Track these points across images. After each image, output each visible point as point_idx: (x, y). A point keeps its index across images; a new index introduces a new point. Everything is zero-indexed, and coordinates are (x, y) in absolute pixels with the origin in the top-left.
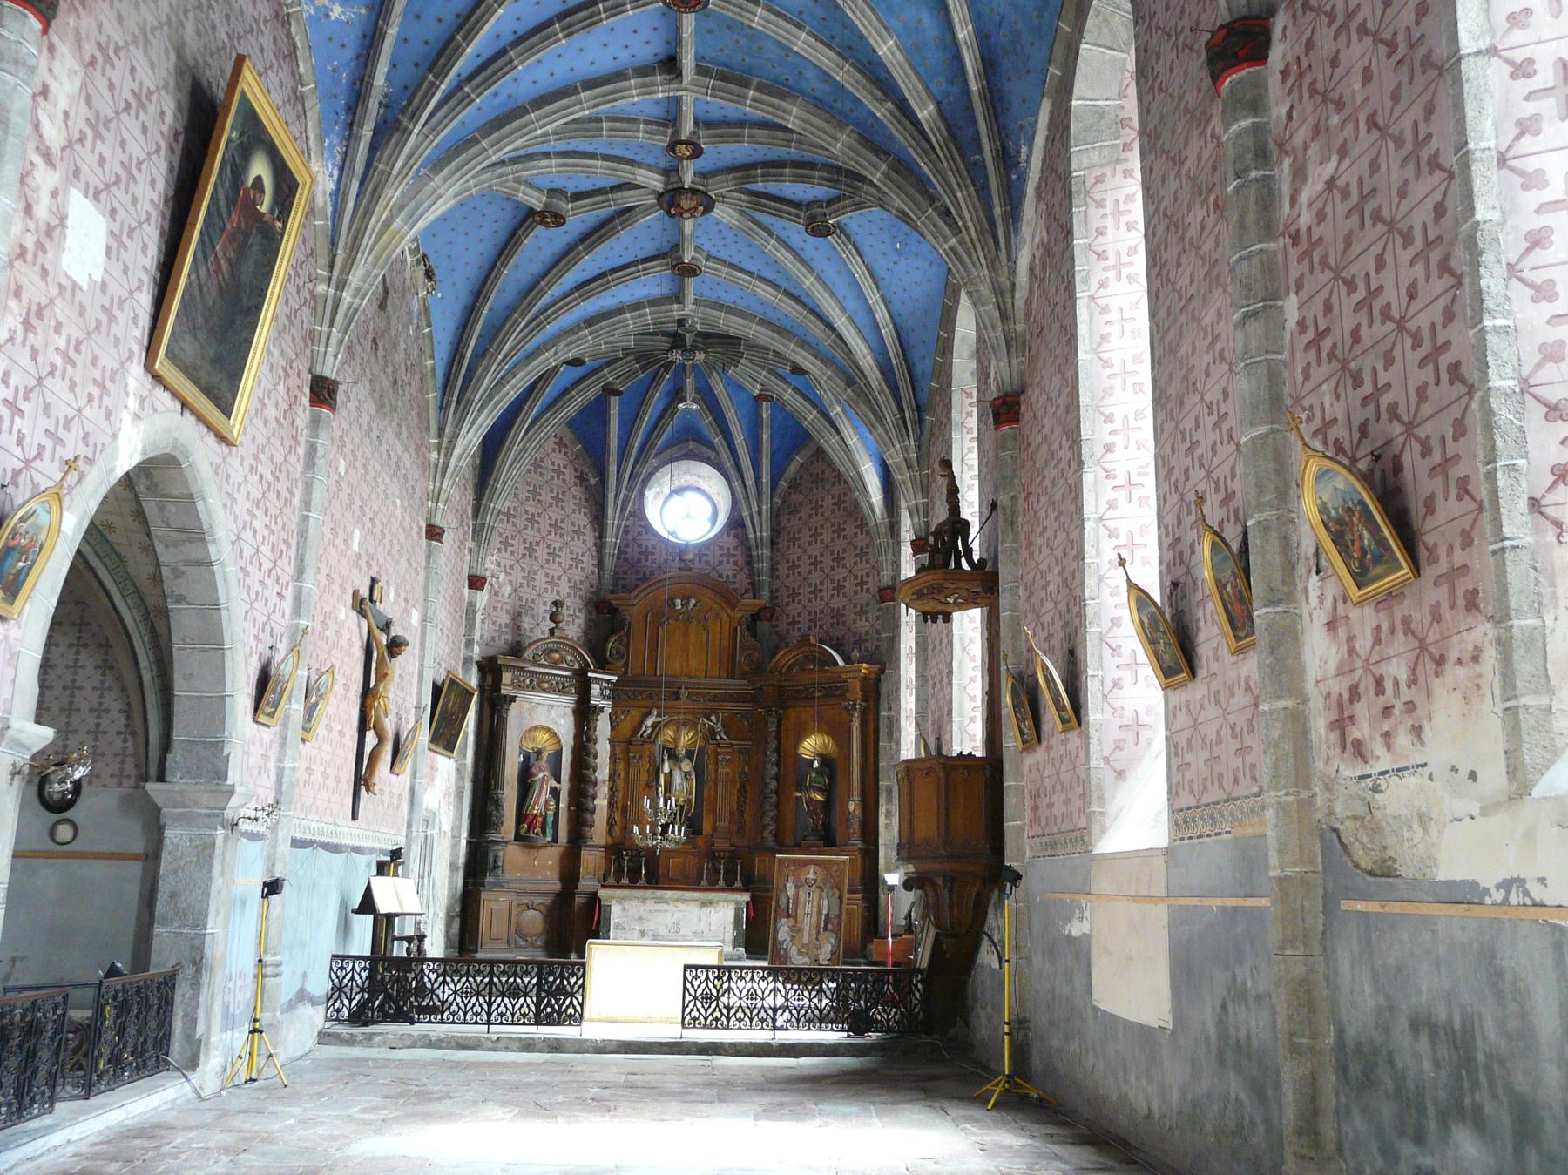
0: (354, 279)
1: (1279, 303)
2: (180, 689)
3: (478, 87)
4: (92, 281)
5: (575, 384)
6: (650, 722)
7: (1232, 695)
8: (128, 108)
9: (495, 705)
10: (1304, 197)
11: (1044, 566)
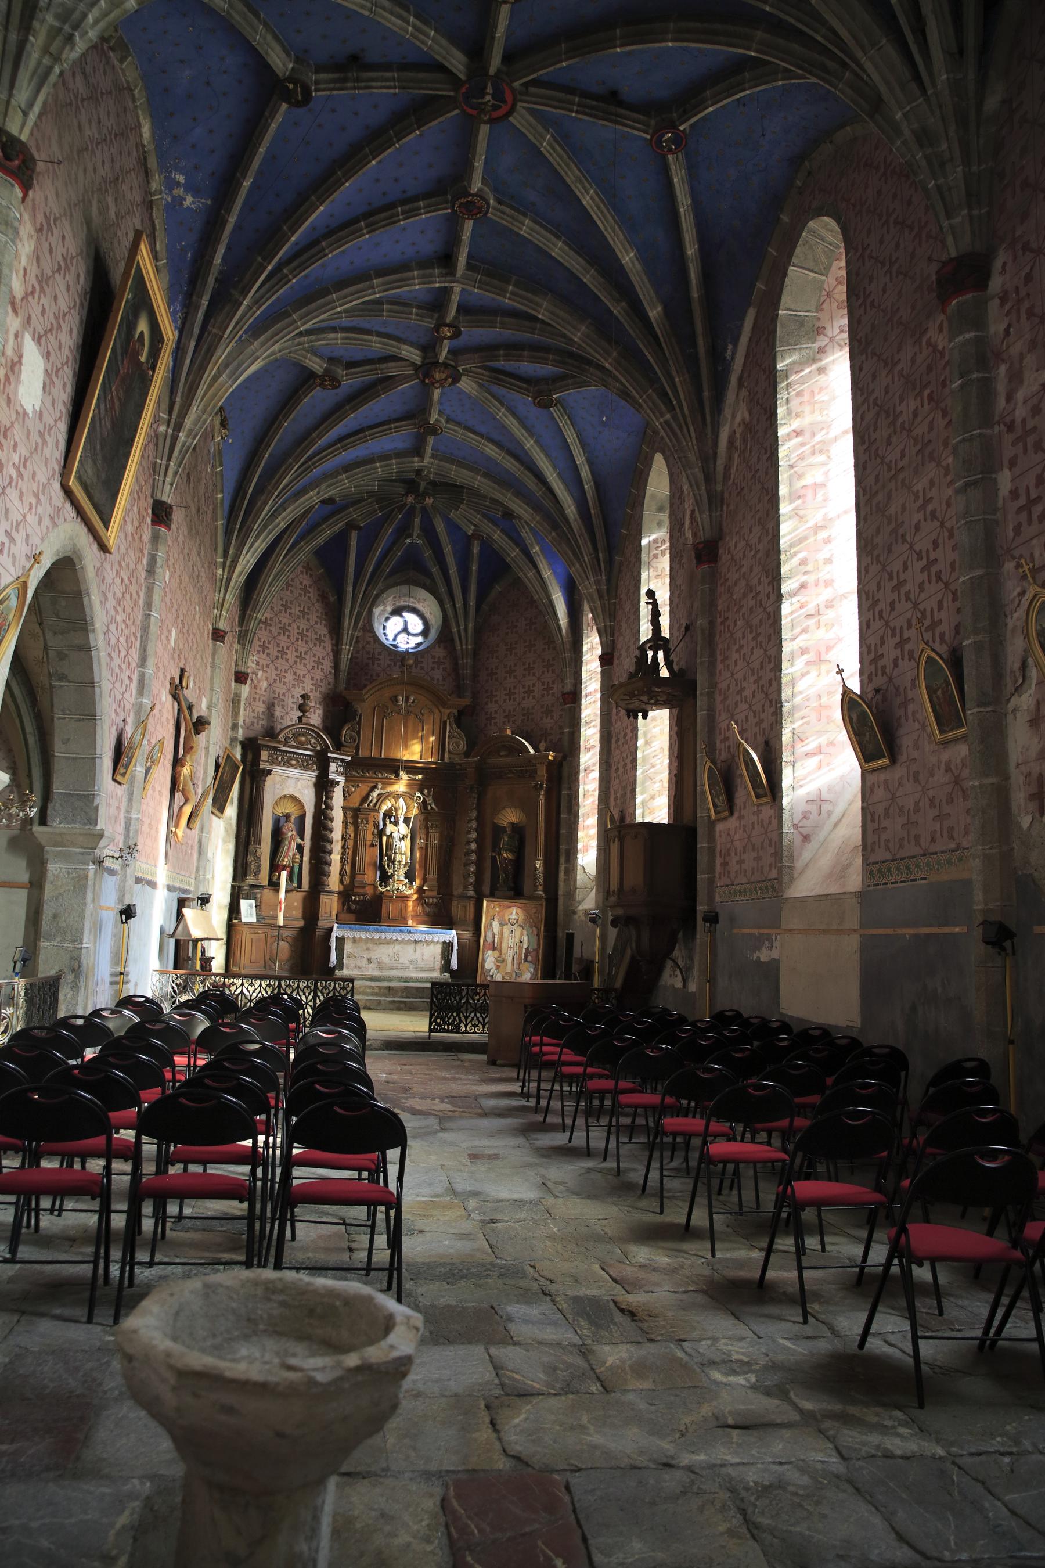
0: (188, 422)
1: (994, 476)
2: (59, 750)
3: (295, 269)
4: (34, 411)
5: (325, 519)
6: (375, 794)
7: (932, 775)
8: (59, 270)
9: (254, 778)
10: (1020, 395)
11: (739, 676)
